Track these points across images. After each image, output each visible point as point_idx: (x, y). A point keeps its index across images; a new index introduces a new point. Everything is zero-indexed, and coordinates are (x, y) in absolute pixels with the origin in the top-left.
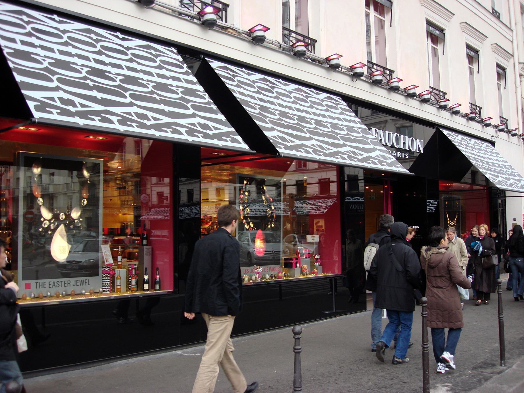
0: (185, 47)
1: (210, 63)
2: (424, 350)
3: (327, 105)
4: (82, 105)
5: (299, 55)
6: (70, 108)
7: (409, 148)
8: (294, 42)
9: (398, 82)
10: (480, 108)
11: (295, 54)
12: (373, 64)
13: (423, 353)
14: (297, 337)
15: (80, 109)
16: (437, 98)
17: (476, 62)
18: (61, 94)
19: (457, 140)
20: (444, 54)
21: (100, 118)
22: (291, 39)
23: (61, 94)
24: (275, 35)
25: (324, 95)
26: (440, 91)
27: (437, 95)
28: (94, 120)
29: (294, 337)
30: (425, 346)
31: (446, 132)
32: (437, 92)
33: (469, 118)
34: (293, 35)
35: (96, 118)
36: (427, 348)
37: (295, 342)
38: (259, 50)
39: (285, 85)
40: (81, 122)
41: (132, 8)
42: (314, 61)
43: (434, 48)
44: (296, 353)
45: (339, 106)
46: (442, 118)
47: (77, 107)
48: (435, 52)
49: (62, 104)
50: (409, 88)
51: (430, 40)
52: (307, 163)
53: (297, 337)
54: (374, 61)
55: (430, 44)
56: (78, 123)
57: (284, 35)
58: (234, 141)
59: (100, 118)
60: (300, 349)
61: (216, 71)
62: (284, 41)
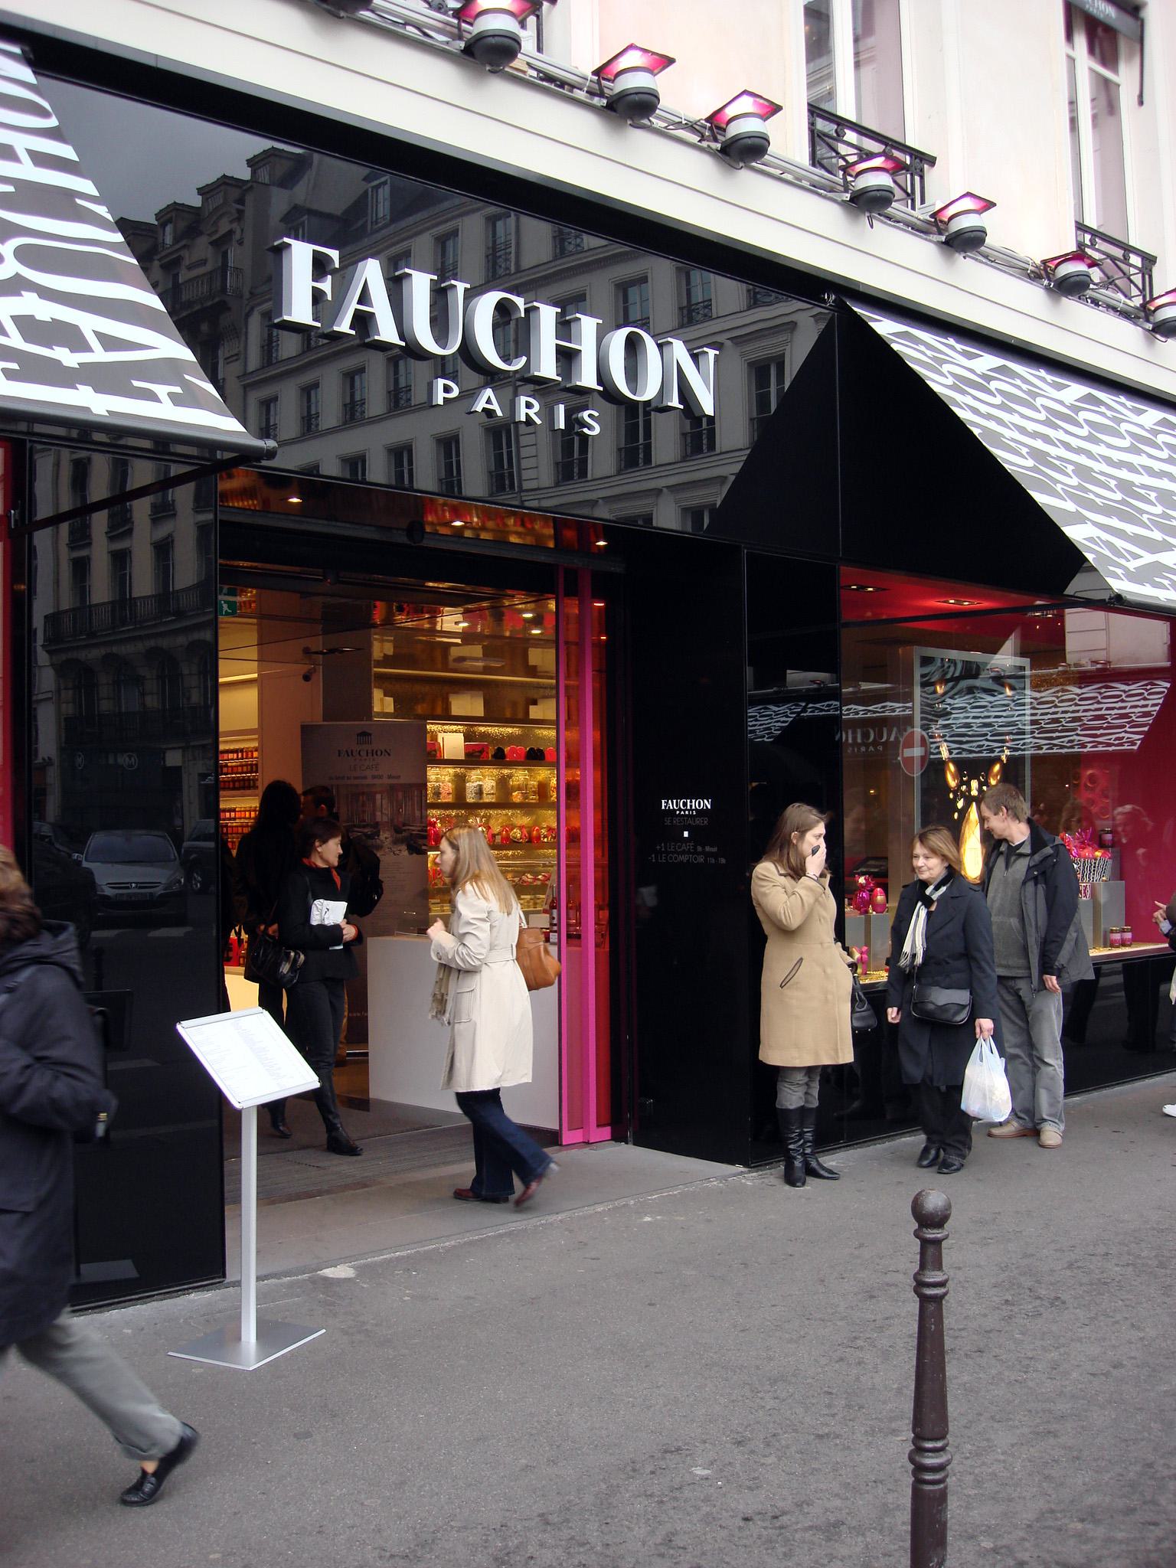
0: (626, 214)
1: (871, 324)
2: (918, 1481)
3: (1121, 436)
4: (110, 343)
5: (868, 204)
6: (68, 358)
7: (603, 375)
8: (852, 159)
9: (979, 212)
10: (1149, 260)
11: (469, 51)
12: (842, 123)
13: (917, 1495)
14: (931, 1234)
15: (99, 355)
16: (872, 172)
17: (1130, 58)
18: (29, 304)
19: (943, 368)
20: (1141, 103)
21: (178, 390)
22: (843, 149)
23: (29, 304)
24: (789, 138)
25: (1076, 390)
26: (1128, 249)
27: (1113, 259)
28: (152, 397)
29: (917, 1234)
30: (930, 1461)
31: (884, 326)
32: (1118, 253)
33: (1061, 283)
34: (851, 136)
35: (162, 390)
36: (940, 1468)
37: (923, 1253)
38: (502, 97)
39: (1060, 387)
40: (98, 404)
41: (296, 27)
42: (554, 85)
43: (1106, 82)
44: (924, 1300)
45: (1124, 427)
46: (883, 259)
47: (86, 348)
48: (1107, 96)
49: (27, 339)
50: (951, 211)
51: (1081, 41)
52: (348, 476)
53: (931, 1234)
54: (846, 109)
55: (1085, 62)
56: (87, 410)
57: (815, 136)
58: (187, 398)
59: (178, 390)
60: (942, 1284)
61: (895, 347)
62: (815, 161)
